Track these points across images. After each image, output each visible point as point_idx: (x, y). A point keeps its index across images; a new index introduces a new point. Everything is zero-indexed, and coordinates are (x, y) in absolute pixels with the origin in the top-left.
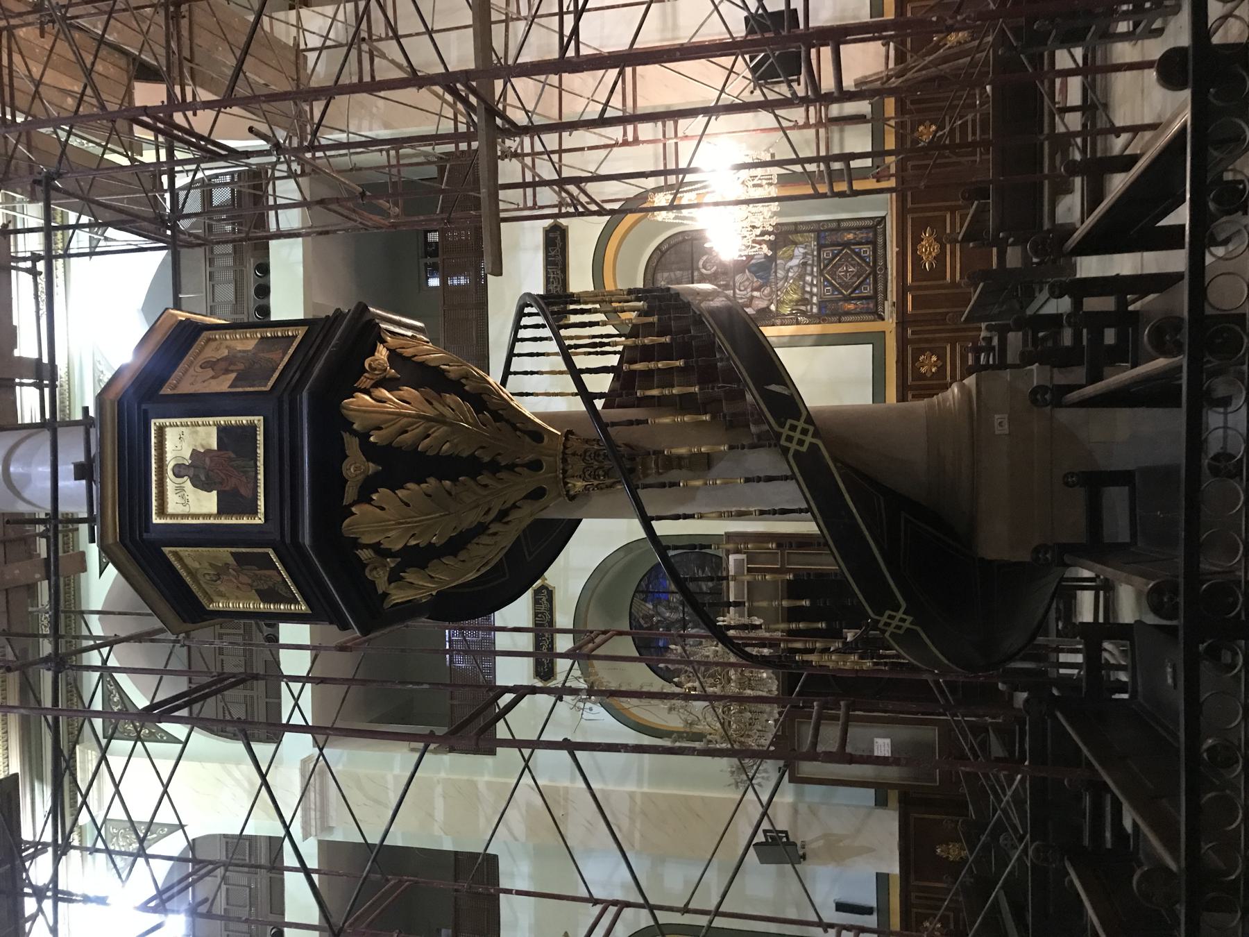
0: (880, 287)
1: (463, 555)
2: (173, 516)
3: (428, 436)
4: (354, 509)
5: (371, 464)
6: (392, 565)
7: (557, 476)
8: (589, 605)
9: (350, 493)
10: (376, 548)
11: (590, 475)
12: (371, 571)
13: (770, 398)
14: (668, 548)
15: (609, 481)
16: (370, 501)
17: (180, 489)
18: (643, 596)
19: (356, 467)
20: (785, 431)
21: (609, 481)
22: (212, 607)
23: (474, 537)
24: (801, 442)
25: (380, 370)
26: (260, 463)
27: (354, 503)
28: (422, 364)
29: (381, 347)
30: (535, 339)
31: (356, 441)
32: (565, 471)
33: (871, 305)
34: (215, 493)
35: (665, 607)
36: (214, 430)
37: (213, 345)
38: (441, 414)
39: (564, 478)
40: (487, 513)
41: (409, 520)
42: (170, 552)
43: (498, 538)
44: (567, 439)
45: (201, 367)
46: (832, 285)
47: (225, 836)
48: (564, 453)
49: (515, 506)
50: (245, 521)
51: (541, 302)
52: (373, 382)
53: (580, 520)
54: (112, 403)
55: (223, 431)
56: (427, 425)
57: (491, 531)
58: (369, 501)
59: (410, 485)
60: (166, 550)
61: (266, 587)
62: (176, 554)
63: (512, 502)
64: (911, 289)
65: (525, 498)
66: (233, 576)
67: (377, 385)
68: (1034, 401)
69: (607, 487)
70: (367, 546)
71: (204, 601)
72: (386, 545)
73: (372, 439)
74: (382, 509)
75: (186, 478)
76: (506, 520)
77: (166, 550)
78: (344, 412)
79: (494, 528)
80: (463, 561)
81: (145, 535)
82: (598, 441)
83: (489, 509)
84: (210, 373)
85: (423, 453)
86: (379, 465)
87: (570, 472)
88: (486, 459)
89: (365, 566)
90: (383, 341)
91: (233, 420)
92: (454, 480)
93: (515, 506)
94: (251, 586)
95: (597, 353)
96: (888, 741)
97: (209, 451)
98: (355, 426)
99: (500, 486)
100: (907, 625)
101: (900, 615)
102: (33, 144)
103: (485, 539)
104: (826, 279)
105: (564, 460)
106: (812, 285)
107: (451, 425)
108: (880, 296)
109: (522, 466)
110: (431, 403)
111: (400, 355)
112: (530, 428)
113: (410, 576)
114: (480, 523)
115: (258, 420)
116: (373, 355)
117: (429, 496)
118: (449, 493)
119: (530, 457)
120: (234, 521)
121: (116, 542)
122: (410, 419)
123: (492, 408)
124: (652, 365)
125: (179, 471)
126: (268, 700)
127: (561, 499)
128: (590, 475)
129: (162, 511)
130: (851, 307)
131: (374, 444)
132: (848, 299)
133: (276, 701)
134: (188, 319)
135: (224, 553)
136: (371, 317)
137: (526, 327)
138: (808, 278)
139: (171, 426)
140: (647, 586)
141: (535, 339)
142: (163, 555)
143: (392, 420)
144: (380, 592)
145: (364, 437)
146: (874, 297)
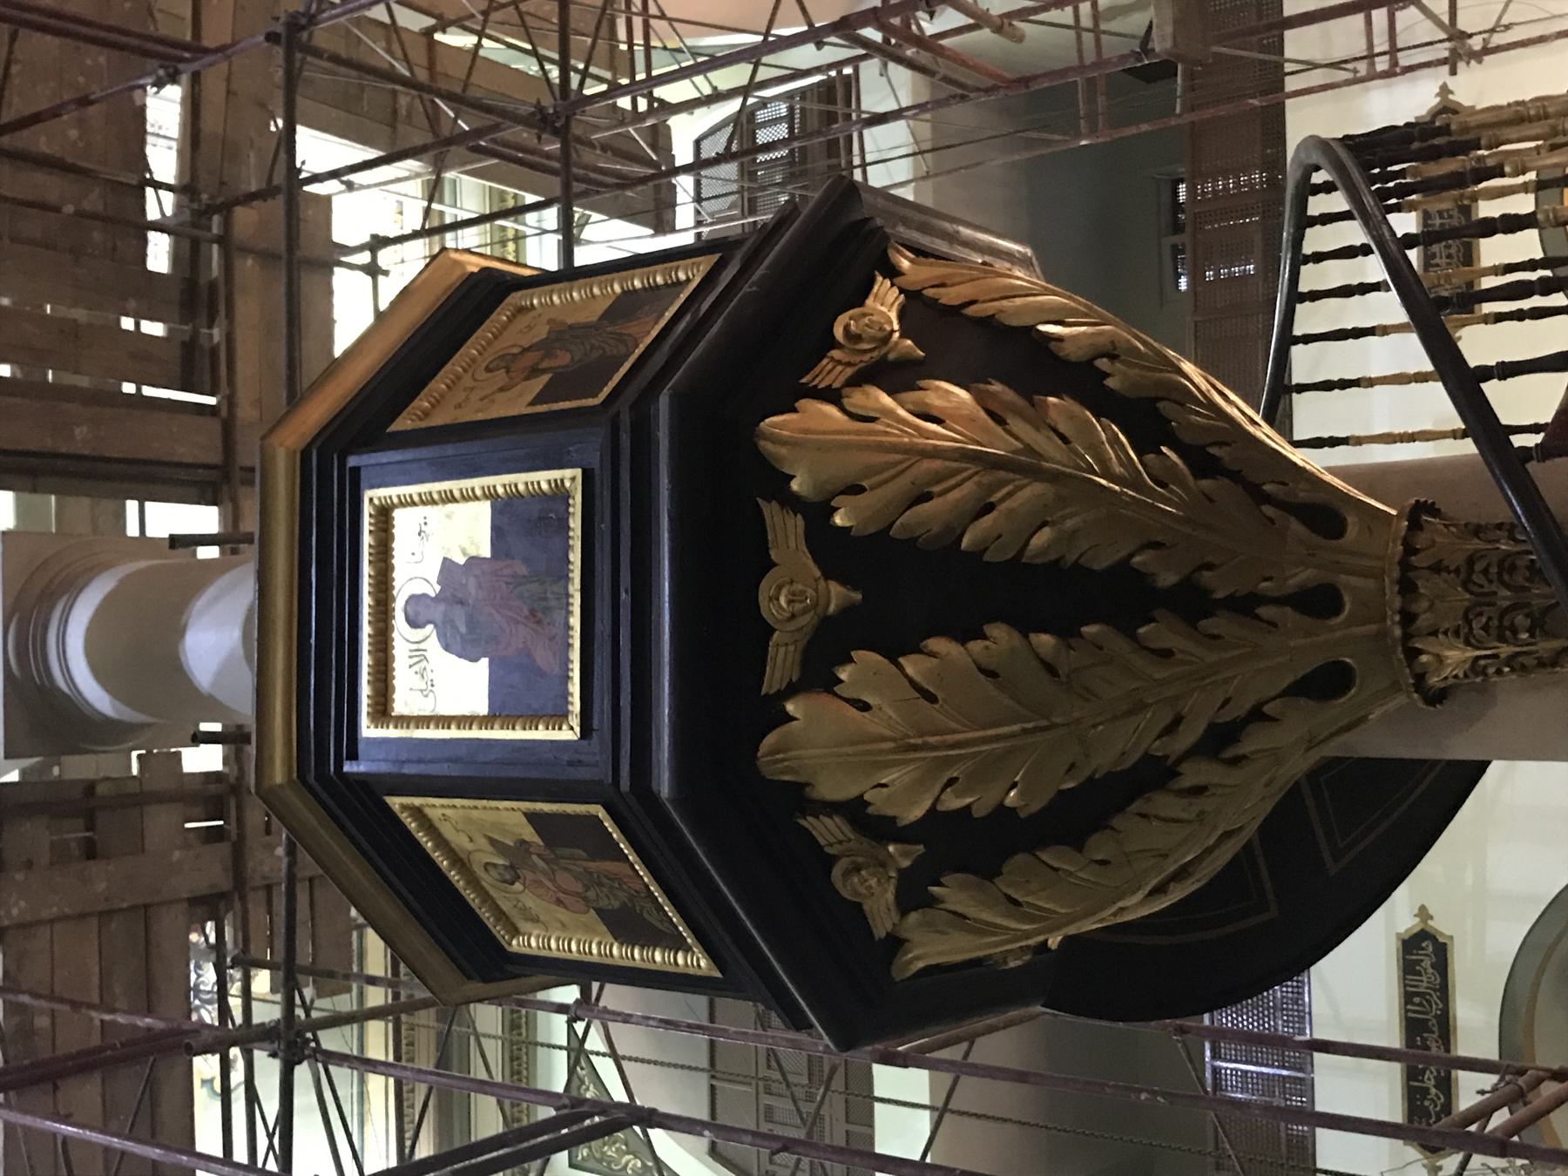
1: (1100, 845)
2: (404, 721)
3: (990, 508)
4: (790, 707)
5: (835, 588)
6: (906, 863)
7: (1384, 634)
8: (1537, 984)
9: (781, 663)
10: (854, 811)
11: (1485, 628)
12: (847, 874)
14: (728, 147)
15: (1546, 647)
21: (1546, 647)
23: (1131, 800)
25: (872, 339)
27: (791, 691)
28: (988, 322)
29: (882, 285)
30: (1346, 292)
31: (796, 524)
32: (1408, 618)
34: (485, 662)
36: (484, 509)
37: (524, 320)
38: (1029, 450)
39: (1407, 637)
40: (1171, 729)
41: (932, 740)
42: (404, 807)
43: (1206, 803)
44: (1415, 524)
45: (488, 370)
48: (1405, 565)
49: (1257, 715)
50: (541, 734)
51: (1344, 155)
52: (849, 371)
53: (1481, 768)
54: (291, 454)
55: (506, 511)
56: (988, 478)
57: (1187, 781)
58: (829, 684)
59: (937, 644)
60: (395, 802)
61: (616, 904)
62: (418, 813)
63: (1248, 706)
65: (1284, 694)
66: (545, 873)
67: (857, 381)
69: (1542, 664)
70: (832, 808)
71: (499, 931)
72: (879, 802)
73: (838, 520)
74: (865, 707)
75: (430, 627)
76: (1229, 753)
77: (395, 802)
78: (766, 446)
79: (1193, 774)
80: (1103, 863)
81: (348, 767)
82: (1511, 530)
83: (1178, 721)
84: (500, 377)
85: (976, 555)
86: (855, 589)
87: (1424, 621)
88: (1167, 579)
89: (831, 860)
90: (893, 272)
92: (1067, 632)
93: (1257, 715)
94: (585, 899)
95: (1519, 316)
97: (473, 560)
98: (795, 486)
99: (1212, 658)
102: (439, 68)
103: (1165, 804)
105: (1407, 587)
107: (1055, 478)
109: (1279, 601)
110: (1000, 421)
111: (934, 302)
112: (1304, 494)
113: (953, 893)
114: (1148, 758)
115: (570, 476)
116: (862, 304)
117: (991, 674)
118: (1051, 669)
119: (1302, 577)
121: (290, 781)
122: (937, 464)
123: (1186, 437)
126: (851, 1128)
127: (1401, 699)
128: (1485, 628)
129: (382, 710)
131: (845, 530)
133: (868, 1131)
134: (484, 270)
135: (510, 816)
136: (866, 213)
137: (1319, 257)
139: (402, 504)
141: (1346, 292)
142: (387, 809)
143: (901, 462)
144: (880, 932)
145: (816, 513)
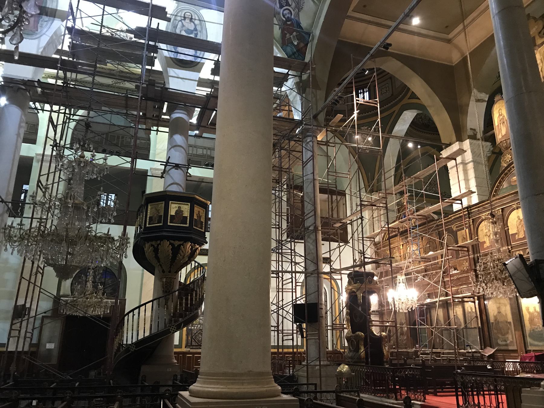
0: (194, 347)
9: (172, 242)
13: (180, 324)
16: (170, 245)
17: (176, 207)
18: (105, 270)
19: (177, 243)
20: (174, 327)
22: (149, 205)
24: (172, 330)
26: (179, 225)
33: (189, 344)
35: (100, 277)
46: (197, 333)
47: (38, 125)
55: (186, 217)
64: (193, 356)
68: (174, 375)
79: (158, 264)
91: (188, 220)
93: (162, 267)
96: (53, 348)
97: (183, 214)
100: (132, 350)
101: (134, 349)
104: (198, 331)
106: (197, 327)
108: (191, 347)
120: (169, 218)
124: (189, 300)
125: (179, 207)
129: (172, 203)
130: (189, 339)
132: (192, 338)
135: (162, 213)
138: (199, 326)
140: (108, 271)
146: (191, 345)
